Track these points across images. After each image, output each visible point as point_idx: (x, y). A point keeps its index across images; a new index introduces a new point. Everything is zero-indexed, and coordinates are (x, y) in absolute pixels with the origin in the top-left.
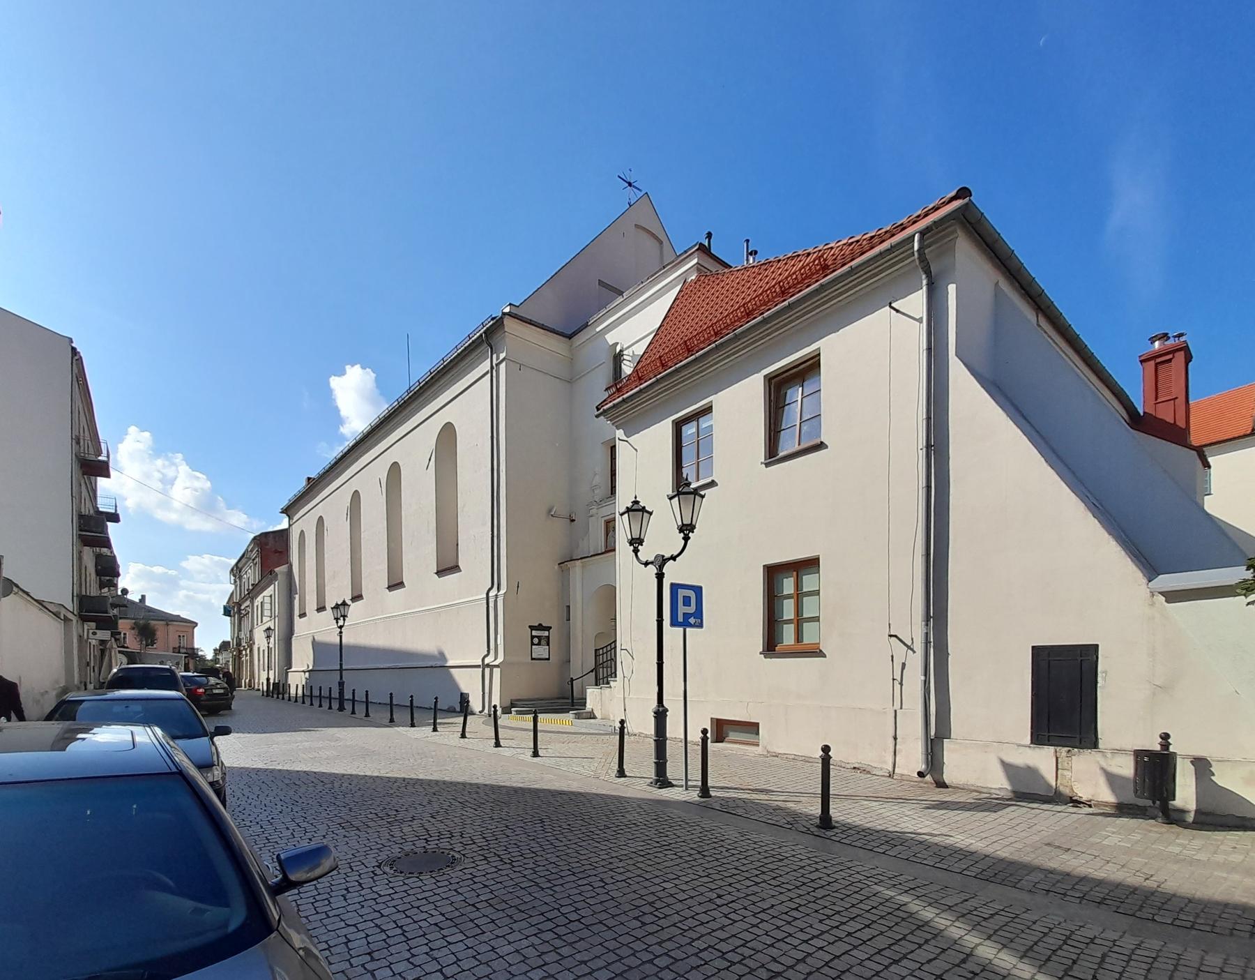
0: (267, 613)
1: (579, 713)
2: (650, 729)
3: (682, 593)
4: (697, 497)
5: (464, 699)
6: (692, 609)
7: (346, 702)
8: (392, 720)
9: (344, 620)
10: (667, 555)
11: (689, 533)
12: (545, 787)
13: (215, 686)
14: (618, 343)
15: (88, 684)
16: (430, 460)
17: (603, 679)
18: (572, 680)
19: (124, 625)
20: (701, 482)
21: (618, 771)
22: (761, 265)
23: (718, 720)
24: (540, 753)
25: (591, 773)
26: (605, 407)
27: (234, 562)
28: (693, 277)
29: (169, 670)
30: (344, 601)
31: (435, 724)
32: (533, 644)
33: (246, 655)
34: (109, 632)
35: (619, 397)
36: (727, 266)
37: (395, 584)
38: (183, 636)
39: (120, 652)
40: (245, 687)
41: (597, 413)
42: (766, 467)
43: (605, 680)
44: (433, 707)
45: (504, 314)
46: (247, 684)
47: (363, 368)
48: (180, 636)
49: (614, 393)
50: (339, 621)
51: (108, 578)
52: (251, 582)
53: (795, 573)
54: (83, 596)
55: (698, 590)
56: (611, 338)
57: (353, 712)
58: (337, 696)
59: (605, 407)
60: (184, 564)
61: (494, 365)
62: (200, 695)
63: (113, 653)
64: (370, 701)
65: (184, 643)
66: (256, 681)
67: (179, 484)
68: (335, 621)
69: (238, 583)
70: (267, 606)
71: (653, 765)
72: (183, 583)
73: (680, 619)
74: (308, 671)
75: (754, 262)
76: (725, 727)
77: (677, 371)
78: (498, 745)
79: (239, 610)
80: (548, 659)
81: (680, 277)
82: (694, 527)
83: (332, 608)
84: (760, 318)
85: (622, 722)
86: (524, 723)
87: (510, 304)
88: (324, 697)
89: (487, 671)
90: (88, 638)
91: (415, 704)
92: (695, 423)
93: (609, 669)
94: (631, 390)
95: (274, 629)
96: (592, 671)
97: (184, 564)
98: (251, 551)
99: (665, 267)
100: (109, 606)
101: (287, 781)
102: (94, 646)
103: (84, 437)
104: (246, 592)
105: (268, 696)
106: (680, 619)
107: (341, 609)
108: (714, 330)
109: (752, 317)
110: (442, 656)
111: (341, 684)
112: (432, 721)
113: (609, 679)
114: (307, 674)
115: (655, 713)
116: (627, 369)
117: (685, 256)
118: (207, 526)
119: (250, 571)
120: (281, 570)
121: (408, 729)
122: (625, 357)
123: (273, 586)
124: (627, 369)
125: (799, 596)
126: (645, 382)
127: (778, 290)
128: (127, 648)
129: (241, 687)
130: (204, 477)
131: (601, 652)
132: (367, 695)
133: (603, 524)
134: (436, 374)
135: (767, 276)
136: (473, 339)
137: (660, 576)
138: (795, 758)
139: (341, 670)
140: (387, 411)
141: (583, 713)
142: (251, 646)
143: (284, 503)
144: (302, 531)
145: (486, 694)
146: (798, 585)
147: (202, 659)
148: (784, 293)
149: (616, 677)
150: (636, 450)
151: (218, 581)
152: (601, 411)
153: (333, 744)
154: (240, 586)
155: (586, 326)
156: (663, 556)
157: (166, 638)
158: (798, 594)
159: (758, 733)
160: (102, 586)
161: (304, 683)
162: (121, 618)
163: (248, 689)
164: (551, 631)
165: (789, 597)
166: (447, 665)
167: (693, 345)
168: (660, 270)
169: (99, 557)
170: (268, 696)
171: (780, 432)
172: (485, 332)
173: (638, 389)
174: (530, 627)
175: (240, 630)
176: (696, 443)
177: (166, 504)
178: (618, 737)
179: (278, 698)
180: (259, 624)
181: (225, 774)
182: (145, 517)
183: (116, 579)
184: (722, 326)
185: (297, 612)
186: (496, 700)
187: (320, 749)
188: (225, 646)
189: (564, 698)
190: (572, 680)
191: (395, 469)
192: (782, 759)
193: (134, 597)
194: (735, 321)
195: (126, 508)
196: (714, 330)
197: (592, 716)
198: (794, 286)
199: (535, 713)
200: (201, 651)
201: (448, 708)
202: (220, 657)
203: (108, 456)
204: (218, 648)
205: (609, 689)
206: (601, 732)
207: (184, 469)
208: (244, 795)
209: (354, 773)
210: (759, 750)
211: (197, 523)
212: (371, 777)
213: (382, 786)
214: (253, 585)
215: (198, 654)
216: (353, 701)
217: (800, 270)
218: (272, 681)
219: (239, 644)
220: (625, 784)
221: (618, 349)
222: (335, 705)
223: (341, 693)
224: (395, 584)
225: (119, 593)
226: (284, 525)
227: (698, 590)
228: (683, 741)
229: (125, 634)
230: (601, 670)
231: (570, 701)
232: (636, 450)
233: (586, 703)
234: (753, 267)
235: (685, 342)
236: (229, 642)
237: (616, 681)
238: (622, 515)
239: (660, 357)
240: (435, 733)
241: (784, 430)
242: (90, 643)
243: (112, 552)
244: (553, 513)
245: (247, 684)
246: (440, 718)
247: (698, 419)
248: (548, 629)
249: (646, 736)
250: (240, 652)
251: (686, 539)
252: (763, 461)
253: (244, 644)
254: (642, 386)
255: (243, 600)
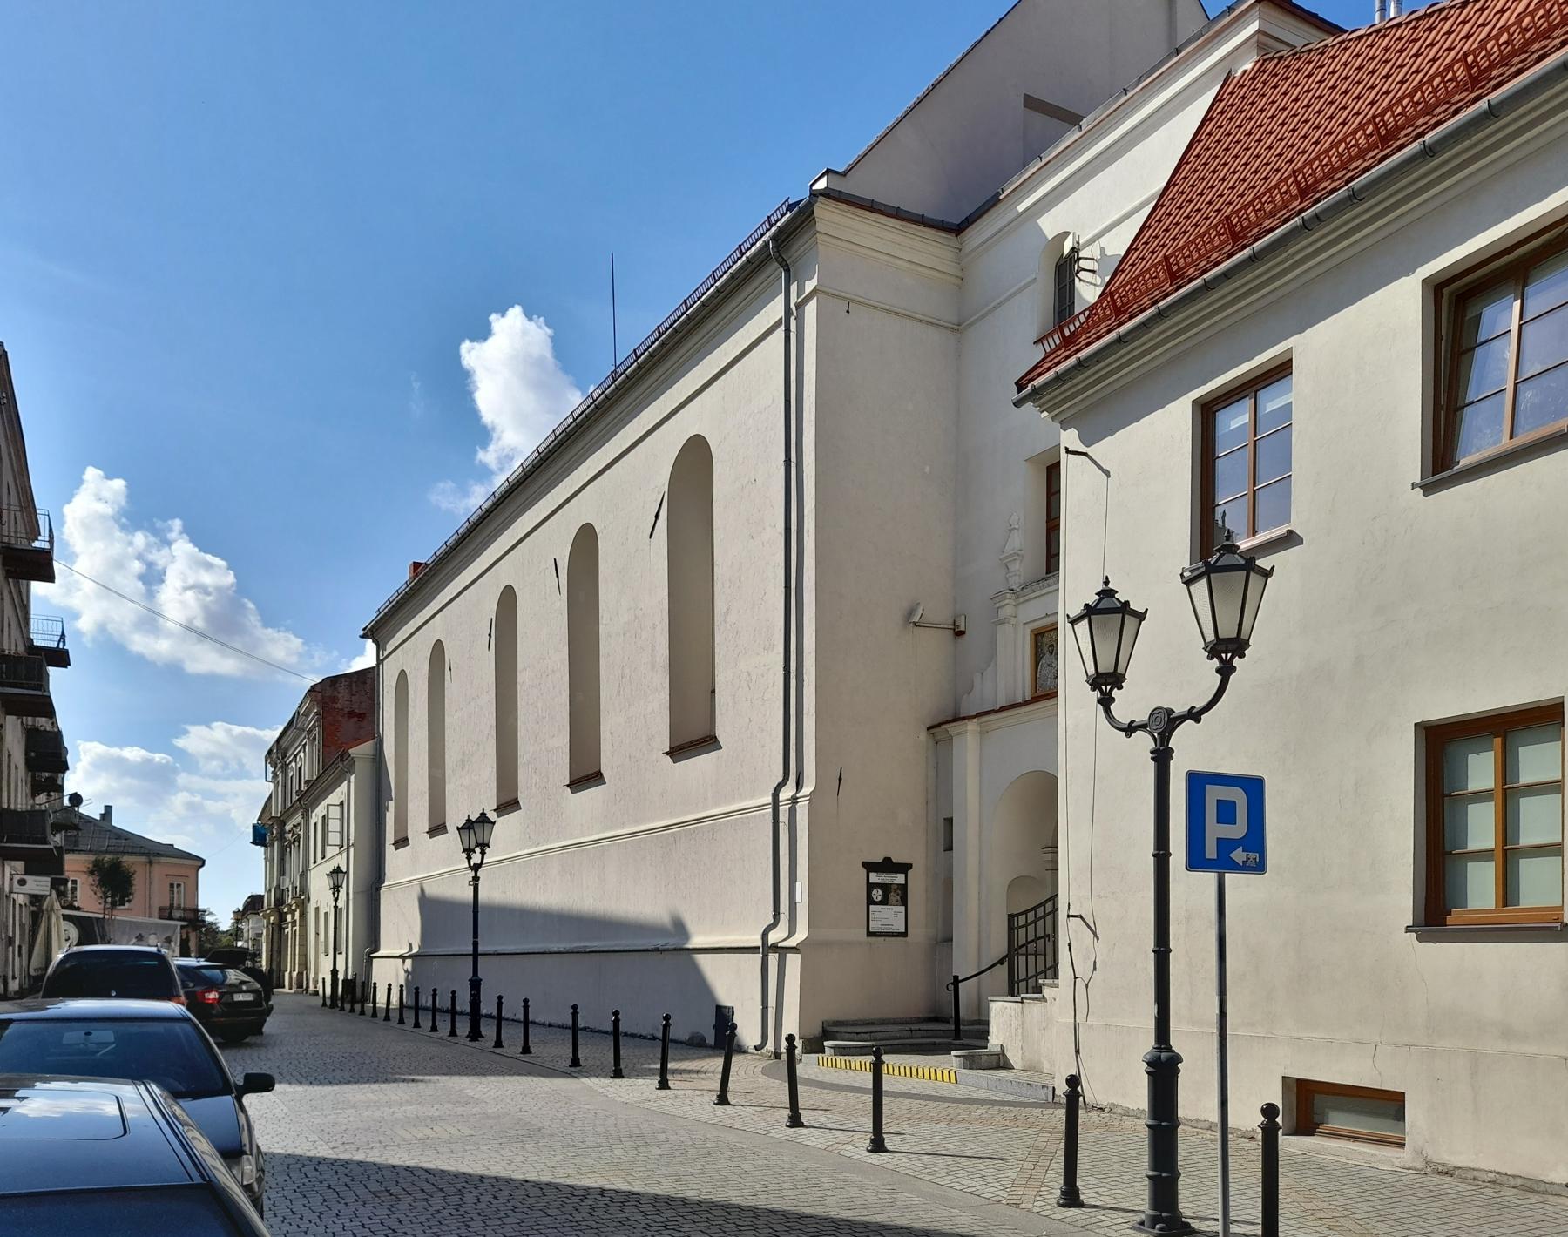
0: (334, 838)
1: (973, 1056)
2: (1137, 1094)
3: (1213, 794)
4: (1252, 574)
5: (724, 1019)
6: (1238, 830)
7: (483, 1022)
8: (575, 1062)
9: (483, 853)
10: (1180, 709)
11: (1232, 658)
12: (900, 1222)
13: (236, 988)
14: (1066, 234)
15: (10, 980)
16: (657, 516)
17: (1026, 980)
18: (956, 981)
19: (75, 865)
20: (1262, 537)
21: (1063, 1193)
22: (1418, 19)
23: (1301, 1083)
24: (888, 1144)
25: (1000, 1193)
26: (1037, 382)
27: (272, 735)
28: (1248, 66)
29: (158, 956)
30: (483, 814)
31: (664, 1072)
32: (870, 902)
33: (294, 923)
34: (49, 879)
35: (1068, 357)
36: (1335, 30)
37: (585, 777)
38: (179, 885)
39: (66, 917)
40: (290, 989)
41: (1016, 396)
42: (1425, 494)
43: (1032, 982)
44: (660, 1035)
45: (815, 195)
46: (294, 981)
47: (529, 315)
48: (172, 885)
49: (1058, 348)
50: (473, 855)
51: (47, 774)
52: (305, 776)
53: (1498, 741)
54: (4, 809)
55: (1254, 787)
56: (1050, 225)
57: (498, 1044)
58: (467, 1009)
59: (1037, 382)
60: (180, 742)
61: (793, 306)
62: (211, 1006)
63: (54, 920)
64: (530, 1019)
65: (180, 899)
66: (312, 975)
67: (173, 581)
68: (465, 855)
69: (280, 778)
70: (334, 825)
71: (1147, 1182)
72: (182, 779)
73: (1211, 852)
74: (410, 957)
75: (1399, 12)
76: (1318, 1098)
77: (1207, 287)
78: (795, 1121)
79: (282, 832)
80: (904, 935)
81: (1215, 70)
82: (1246, 644)
83: (458, 829)
84: (1414, 147)
85: (1073, 1081)
86: (851, 1073)
87: (828, 172)
88: (462, 1013)
89: (773, 959)
90: (11, 892)
91: (622, 1028)
92: (1248, 403)
93: (1040, 958)
94: (1099, 338)
95: (347, 873)
96: (1001, 962)
97: (180, 742)
98: (306, 714)
99: (1176, 51)
100: (48, 830)
101: (374, 1186)
102: (20, 905)
103: (9, 504)
104: (295, 798)
105: (333, 1005)
106: (1211, 852)
107: (476, 831)
108: (1298, 183)
109: (1074, 348)
110: (680, 928)
111: (475, 984)
112: (659, 1066)
113: (1041, 981)
114: (409, 962)
115: (1149, 1064)
116: (1088, 291)
117: (1227, 19)
118: (227, 665)
119: (302, 754)
120: (361, 751)
121: (608, 1081)
122: (1083, 263)
123: (346, 782)
124: (1088, 291)
125: (1508, 795)
126: (1131, 318)
127: (1460, 74)
128: (78, 909)
129: (284, 987)
130: (223, 563)
131: (1022, 920)
132: (526, 1008)
133: (1028, 638)
134: (670, 336)
135: (1432, 45)
136: (748, 254)
137: (1162, 757)
138: (1498, 1181)
139: (475, 955)
140: (571, 419)
141: (980, 1055)
142: (303, 904)
143: (369, 617)
144: (403, 671)
145: (770, 1010)
146: (1507, 768)
147: (212, 930)
148: (1477, 80)
149: (1056, 976)
150: (1107, 473)
151: (242, 773)
152: (1028, 390)
153: (460, 1110)
154: (284, 786)
155: (994, 201)
156: (1170, 711)
157: (149, 888)
158: (1505, 791)
159: (1400, 1115)
160: (36, 789)
161: (402, 982)
162: (68, 851)
163: (295, 993)
164: (910, 873)
165: (1482, 796)
166: (690, 946)
167: (1245, 223)
168: (1169, 57)
169: (32, 735)
170: (333, 1005)
171: (1463, 408)
172: (773, 238)
173: (1113, 335)
174: (865, 864)
175: (282, 873)
176: (1251, 446)
177: (151, 620)
178: (1061, 1114)
179: (352, 1010)
180: (319, 860)
181: (263, 1171)
182: (111, 647)
183: (61, 775)
184: (1319, 173)
185: (390, 837)
186: (791, 1025)
187: (435, 1120)
188: (254, 904)
189: (936, 1020)
190: (956, 981)
191: (586, 540)
192: (1462, 1179)
193: (91, 809)
194: (1352, 159)
195: (79, 633)
196: (1298, 183)
197: (1000, 1062)
198: (1505, 61)
199: (878, 1054)
200: (211, 913)
201: (691, 1038)
202: (244, 926)
203: (51, 541)
204: (241, 909)
205: (1039, 1005)
206: (1022, 1099)
207: (183, 547)
208: (294, 1213)
209: (503, 1174)
210: (1404, 1157)
211: (208, 660)
212: (536, 1184)
213: (557, 1204)
214: (307, 782)
215: (204, 921)
216: (499, 1018)
217: (1520, 19)
218: (341, 977)
219: (280, 901)
220: (1080, 1223)
221: (1068, 245)
222: (463, 1027)
223: (475, 1002)
224: (585, 777)
225: (66, 802)
226: (366, 658)
227: (1254, 787)
228: (1219, 1129)
229: (74, 882)
230: (1022, 959)
231: (953, 1027)
232: (1107, 473)
233: (987, 1032)
234: (1399, 25)
235: (1228, 218)
236: (262, 897)
237: (1057, 986)
238: (1074, 622)
239: (1166, 258)
240: (664, 1092)
241: (1473, 403)
242: (14, 900)
243: (55, 724)
244: (916, 619)
245: (294, 981)
246: (674, 1060)
247: (1256, 392)
248: (904, 868)
249: (1128, 1113)
250: (282, 917)
251: (1226, 671)
252: (1418, 480)
253: (289, 901)
254: (1122, 329)
255: (288, 813)
